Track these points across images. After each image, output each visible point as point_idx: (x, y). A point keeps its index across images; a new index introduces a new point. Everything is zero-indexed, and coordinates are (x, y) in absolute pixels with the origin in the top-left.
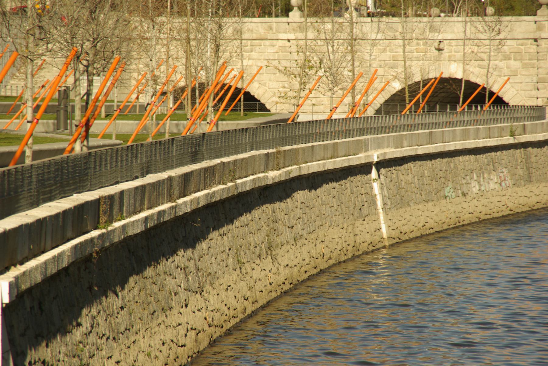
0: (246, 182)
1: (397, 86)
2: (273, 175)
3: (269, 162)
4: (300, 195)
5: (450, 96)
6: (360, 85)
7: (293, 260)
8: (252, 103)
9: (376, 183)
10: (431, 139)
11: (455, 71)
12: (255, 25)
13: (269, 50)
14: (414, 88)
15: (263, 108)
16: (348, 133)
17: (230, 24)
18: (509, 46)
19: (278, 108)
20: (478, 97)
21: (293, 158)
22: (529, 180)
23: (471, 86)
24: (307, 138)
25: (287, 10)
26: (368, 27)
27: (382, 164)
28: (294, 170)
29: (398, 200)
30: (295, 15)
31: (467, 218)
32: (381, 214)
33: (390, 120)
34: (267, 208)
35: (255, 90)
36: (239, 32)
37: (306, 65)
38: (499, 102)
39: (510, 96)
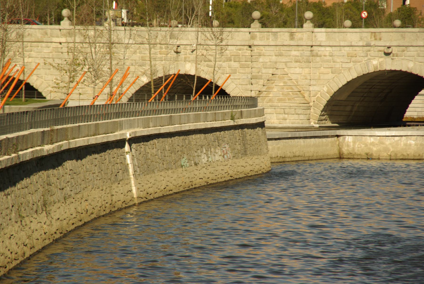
0: (27, 154)
1: (145, 80)
2: (48, 148)
3: (44, 138)
4: (69, 164)
5: (186, 88)
6: (117, 78)
7: (63, 215)
8: (31, 92)
9: (128, 154)
10: (171, 122)
11: (189, 69)
12: (34, 31)
13: (46, 50)
14: (158, 82)
15: (40, 95)
16: (107, 116)
17: (14, 30)
18: (231, 51)
19: (52, 95)
20: (206, 90)
21: (63, 135)
22: (245, 153)
23: (202, 81)
24: (75, 119)
25: (59, 20)
26: (122, 34)
27: (135, 140)
28: (64, 145)
29: (145, 168)
30: (65, 24)
31: (198, 182)
32: (133, 179)
33: (139, 107)
34: (43, 174)
35: (34, 82)
36: (21, 36)
37: (75, 63)
38: (223, 93)
39: (231, 89)
